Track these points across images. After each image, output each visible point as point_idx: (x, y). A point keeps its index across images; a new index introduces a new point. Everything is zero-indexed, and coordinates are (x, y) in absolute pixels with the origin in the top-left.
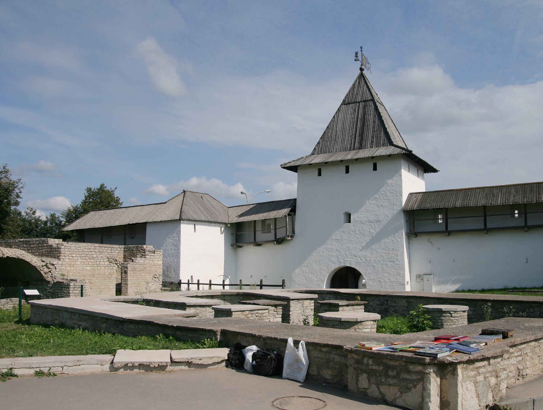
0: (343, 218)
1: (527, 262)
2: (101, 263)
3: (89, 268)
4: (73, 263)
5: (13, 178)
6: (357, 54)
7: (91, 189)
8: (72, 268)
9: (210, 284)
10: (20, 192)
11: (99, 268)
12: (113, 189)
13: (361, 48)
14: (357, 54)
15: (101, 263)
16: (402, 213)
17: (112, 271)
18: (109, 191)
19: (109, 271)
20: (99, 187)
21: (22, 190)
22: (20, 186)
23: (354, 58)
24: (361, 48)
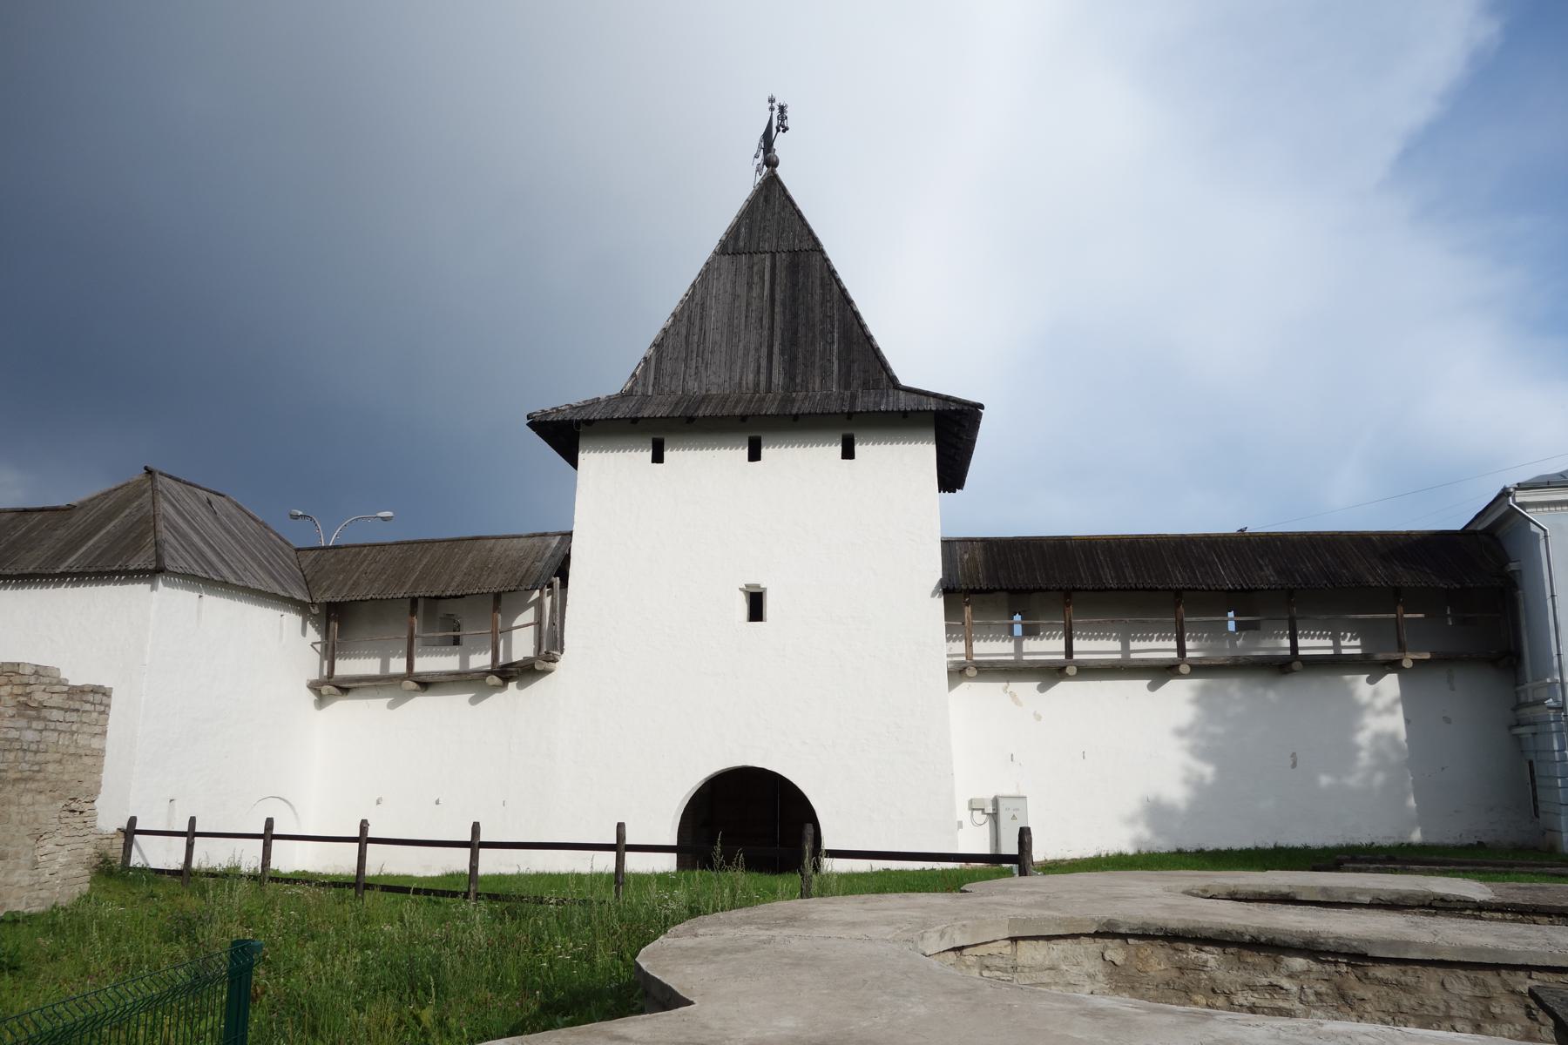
1: (1294, 765)
9: (191, 834)
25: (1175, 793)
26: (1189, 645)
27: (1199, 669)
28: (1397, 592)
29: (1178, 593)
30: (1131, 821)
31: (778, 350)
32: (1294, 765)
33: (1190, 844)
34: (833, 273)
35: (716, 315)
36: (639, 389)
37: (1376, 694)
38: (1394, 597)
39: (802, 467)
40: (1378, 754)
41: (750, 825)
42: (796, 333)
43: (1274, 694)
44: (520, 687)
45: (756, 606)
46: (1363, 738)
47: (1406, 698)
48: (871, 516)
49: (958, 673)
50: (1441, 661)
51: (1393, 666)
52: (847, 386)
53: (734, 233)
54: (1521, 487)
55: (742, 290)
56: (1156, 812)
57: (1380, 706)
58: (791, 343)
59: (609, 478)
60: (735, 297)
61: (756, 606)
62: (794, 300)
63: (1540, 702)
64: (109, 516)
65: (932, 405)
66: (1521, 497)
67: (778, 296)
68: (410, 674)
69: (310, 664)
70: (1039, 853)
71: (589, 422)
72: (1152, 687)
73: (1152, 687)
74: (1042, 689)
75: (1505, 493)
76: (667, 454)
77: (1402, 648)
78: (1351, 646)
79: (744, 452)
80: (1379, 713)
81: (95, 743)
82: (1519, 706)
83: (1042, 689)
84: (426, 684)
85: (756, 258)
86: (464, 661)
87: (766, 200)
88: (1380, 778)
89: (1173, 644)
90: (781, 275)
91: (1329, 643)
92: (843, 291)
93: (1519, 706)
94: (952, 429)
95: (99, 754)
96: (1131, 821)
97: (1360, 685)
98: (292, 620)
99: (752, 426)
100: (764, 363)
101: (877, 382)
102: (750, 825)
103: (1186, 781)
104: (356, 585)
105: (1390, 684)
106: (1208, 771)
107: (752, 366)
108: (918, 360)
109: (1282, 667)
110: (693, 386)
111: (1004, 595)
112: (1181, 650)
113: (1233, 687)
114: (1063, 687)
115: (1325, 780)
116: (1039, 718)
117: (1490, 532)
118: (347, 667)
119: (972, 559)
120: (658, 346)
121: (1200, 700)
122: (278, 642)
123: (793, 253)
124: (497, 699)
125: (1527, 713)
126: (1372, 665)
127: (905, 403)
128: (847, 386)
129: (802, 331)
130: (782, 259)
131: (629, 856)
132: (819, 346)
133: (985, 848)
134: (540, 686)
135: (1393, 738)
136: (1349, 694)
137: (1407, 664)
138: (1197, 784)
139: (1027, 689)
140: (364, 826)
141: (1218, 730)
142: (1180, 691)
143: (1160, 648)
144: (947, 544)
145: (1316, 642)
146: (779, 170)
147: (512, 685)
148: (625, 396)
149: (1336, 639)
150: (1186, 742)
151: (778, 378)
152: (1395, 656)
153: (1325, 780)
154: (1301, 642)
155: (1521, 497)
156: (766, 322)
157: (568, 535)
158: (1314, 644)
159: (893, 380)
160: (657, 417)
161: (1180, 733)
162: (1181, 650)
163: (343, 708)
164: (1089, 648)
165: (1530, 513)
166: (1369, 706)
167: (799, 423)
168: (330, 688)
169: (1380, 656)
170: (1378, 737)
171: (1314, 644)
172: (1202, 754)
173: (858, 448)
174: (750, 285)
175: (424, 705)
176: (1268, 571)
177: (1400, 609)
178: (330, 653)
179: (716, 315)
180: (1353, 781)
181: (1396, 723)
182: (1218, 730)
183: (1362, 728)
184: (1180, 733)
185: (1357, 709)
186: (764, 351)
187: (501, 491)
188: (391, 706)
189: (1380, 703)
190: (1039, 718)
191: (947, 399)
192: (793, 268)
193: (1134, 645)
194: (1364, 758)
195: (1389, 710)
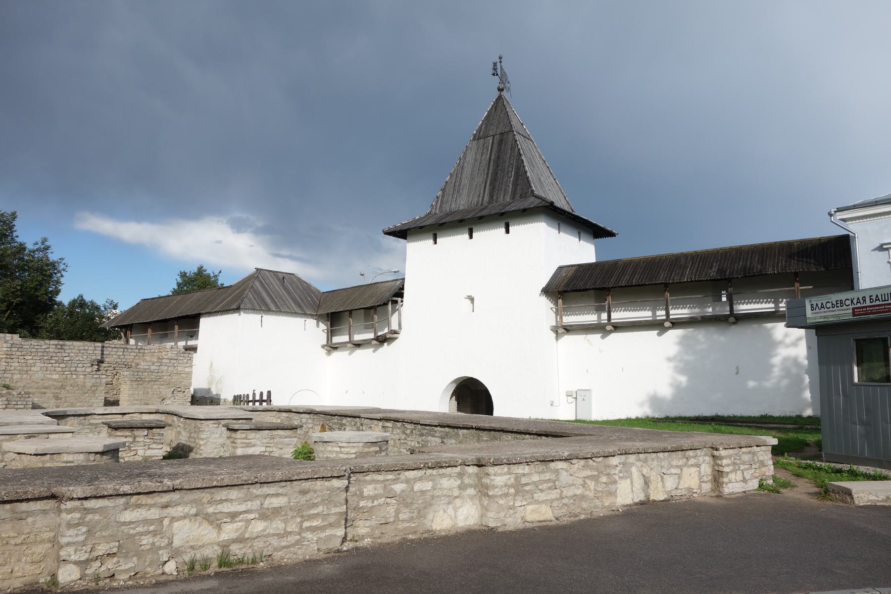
1: (737, 373)
2: (78, 369)
3: (56, 377)
4: (25, 369)
5: (53, 257)
6: (495, 64)
7: (185, 273)
8: (25, 376)
10: (62, 276)
11: (74, 377)
12: (216, 273)
13: (500, 58)
14: (495, 64)
15: (78, 369)
16: (544, 299)
17: (98, 380)
18: (209, 276)
19: (93, 381)
20: (196, 270)
21: (63, 273)
22: (62, 267)
23: (492, 71)
24: (500, 58)
25: (665, 391)
30: (642, 405)
32: (737, 373)
33: (673, 414)
37: (786, 335)
44: (388, 345)
46: (776, 360)
55: (478, 157)
56: (655, 400)
58: (494, 180)
59: (418, 251)
62: (499, 158)
64: (238, 288)
67: (493, 157)
68: (350, 342)
69: (323, 338)
71: (409, 229)
79: (503, 230)
80: (787, 346)
81: (187, 370)
88: (785, 382)
90: (495, 146)
91: (772, 305)
95: (190, 374)
96: (642, 405)
97: (779, 329)
98: (311, 322)
100: (482, 192)
103: (671, 385)
106: (683, 379)
111: (592, 291)
113: (701, 335)
115: (751, 384)
116: (601, 351)
118: (336, 339)
121: (683, 342)
122: (312, 331)
129: (499, 172)
132: (505, 180)
133: (573, 418)
135: (795, 361)
136: (769, 334)
138: (677, 387)
139: (596, 337)
142: (674, 335)
145: (680, 311)
147: (386, 344)
149: (776, 303)
150: (672, 364)
151: (486, 198)
153: (751, 384)
154: (671, 312)
157: (404, 279)
161: (669, 359)
163: (336, 354)
166: (780, 343)
168: (332, 348)
170: (786, 359)
172: (681, 371)
177: (797, 285)
178: (331, 333)
180: (768, 384)
182: (687, 358)
183: (776, 355)
184: (669, 359)
185: (772, 345)
190: (601, 351)
194: (776, 371)
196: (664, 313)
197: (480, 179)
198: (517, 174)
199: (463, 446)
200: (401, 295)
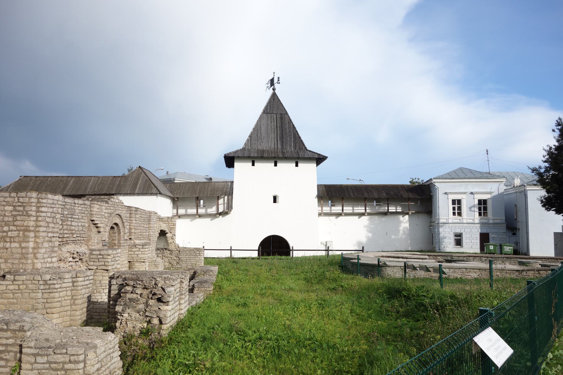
0: (279, 199)
9: (231, 250)
25: (364, 240)
26: (367, 208)
27: (369, 214)
28: (409, 198)
29: (365, 198)
31: (277, 138)
34: (291, 120)
35: (263, 129)
36: (247, 148)
38: (409, 200)
39: (286, 167)
40: (404, 232)
41: (274, 246)
42: (283, 135)
43: (384, 219)
45: (275, 199)
46: (401, 228)
47: (409, 220)
48: (303, 180)
49: (320, 215)
50: (417, 213)
51: (408, 214)
52: (295, 149)
53: (266, 108)
54: (434, 179)
55: (269, 123)
57: (405, 222)
58: (282, 137)
60: (268, 125)
61: (275, 199)
63: (434, 222)
65: (316, 156)
66: (434, 180)
70: (365, 250)
72: (359, 218)
73: (359, 218)
74: (336, 218)
75: (431, 180)
76: (255, 164)
77: (409, 210)
78: (399, 209)
79: (273, 164)
82: (431, 222)
83: (336, 218)
84: (200, 216)
85: (272, 115)
86: (206, 210)
87: (273, 99)
88: (404, 236)
89: (364, 208)
90: (279, 120)
91: (351, 208)
92: (293, 125)
93: (431, 222)
94: (319, 159)
97: (401, 217)
99: (275, 158)
101: (302, 148)
102: (274, 246)
104: (184, 193)
105: (407, 217)
106: (370, 235)
107: (273, 143)
108: (311, 143)
109: (386, 214)
110: (260, 147)
112: (366, 210)
113: (376, 218)
114: (341, 218)
115: (393, 237)
117: (428, 185)
119: (323, 190)
120: (250, 136)
123: (281, 114)
124: (217, 219)
125: (432, 224)
126: (403, 213)
127: (310, 155)
128: (295, 149)
130: (279, 116)
131: (330, 252)
132: (289, 139)
134: (227, 217)
135: (407, 228)
136: (399, 219)
137: (410, 213)
138: (368, 238)
139: (333, 218)
140: (231, 247)
141: (372, 226)
142: (365, 219)
143: (361, 209)
144: (319, 186)
146: (276, 91)
148: (243, 149)
149: (396, 207)
150: (366, 229)
151: (279, 146)
152: (408, 212)
153: (393, 237)
155: (434, 180)
156: (276, 132)
158: (392, 209)
159: (306, 148)
160: (253, 153)
161: (365, 227)
162: (366, 210)
164: (348, 209)
165: (436, 184)
167: (286, 159)
169: (406, 212)
170: (404, 228)
171: (392, 209)
172: (370, 231)
173: (299, 164)
174: (271, 122)
175: (199, 221)
176: (384, 194)
179: (263, 129)
181: (407, 225)
182: (372, 226)
184: (365, 227)
185: (400, 222)
186: (276, 139)
187: (221, 174)
188: (191, 221)
189: (405, 221)
191: (319, 154)
192: (281, 118)
193: (355, 208)
194: (401, 232)
195: (406, 222)
196: (341, 208)
197: (273, 136)
198: (294, 136)
199: (422, 284)
200: (130, 207)
